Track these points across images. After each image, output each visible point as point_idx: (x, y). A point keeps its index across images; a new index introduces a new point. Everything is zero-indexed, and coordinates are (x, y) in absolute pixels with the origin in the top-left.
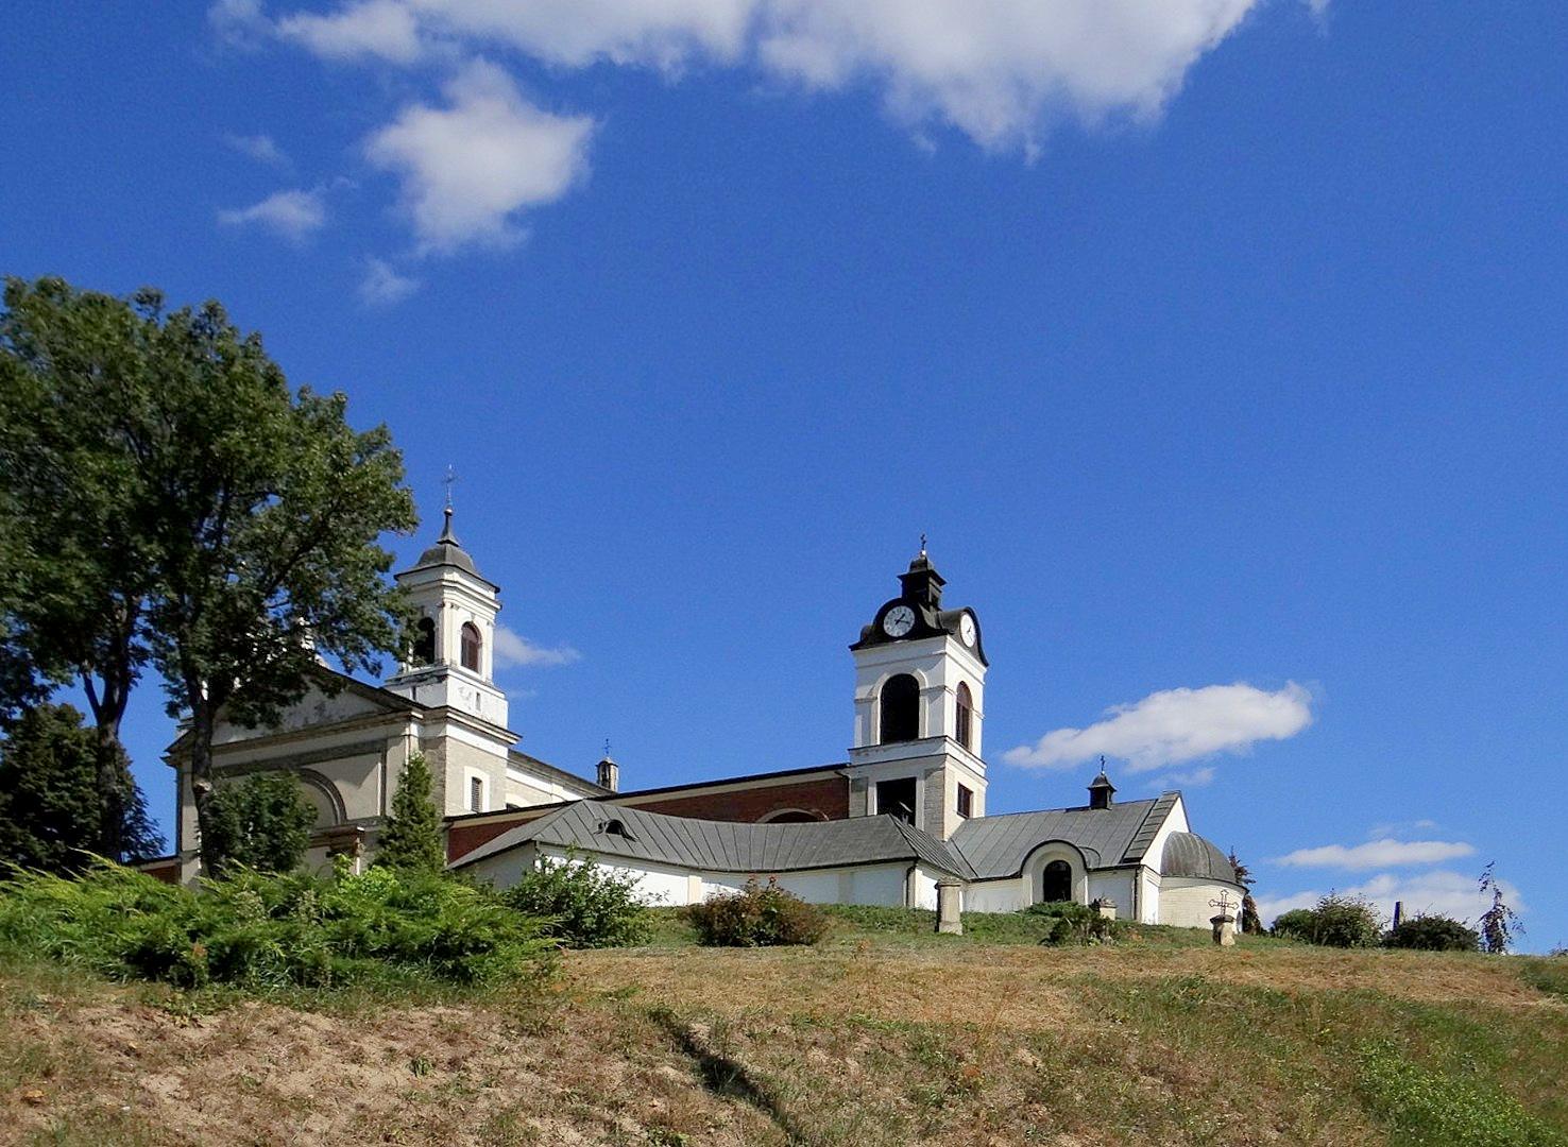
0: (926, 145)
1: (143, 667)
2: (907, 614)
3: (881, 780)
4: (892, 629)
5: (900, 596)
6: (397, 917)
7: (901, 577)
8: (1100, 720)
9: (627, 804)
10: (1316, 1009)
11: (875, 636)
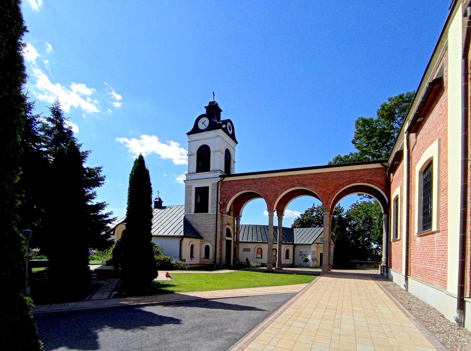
0: (136, 169)
1: (299, 216)
2: (206, 120)
3: (196, 187)
4: (201, 126)
5: (205, 113)
6: (59, 308)
7: (206, 107)
8: (391, 183)
9: (170, 295)
10: (190, 206)
11: (196, 130)
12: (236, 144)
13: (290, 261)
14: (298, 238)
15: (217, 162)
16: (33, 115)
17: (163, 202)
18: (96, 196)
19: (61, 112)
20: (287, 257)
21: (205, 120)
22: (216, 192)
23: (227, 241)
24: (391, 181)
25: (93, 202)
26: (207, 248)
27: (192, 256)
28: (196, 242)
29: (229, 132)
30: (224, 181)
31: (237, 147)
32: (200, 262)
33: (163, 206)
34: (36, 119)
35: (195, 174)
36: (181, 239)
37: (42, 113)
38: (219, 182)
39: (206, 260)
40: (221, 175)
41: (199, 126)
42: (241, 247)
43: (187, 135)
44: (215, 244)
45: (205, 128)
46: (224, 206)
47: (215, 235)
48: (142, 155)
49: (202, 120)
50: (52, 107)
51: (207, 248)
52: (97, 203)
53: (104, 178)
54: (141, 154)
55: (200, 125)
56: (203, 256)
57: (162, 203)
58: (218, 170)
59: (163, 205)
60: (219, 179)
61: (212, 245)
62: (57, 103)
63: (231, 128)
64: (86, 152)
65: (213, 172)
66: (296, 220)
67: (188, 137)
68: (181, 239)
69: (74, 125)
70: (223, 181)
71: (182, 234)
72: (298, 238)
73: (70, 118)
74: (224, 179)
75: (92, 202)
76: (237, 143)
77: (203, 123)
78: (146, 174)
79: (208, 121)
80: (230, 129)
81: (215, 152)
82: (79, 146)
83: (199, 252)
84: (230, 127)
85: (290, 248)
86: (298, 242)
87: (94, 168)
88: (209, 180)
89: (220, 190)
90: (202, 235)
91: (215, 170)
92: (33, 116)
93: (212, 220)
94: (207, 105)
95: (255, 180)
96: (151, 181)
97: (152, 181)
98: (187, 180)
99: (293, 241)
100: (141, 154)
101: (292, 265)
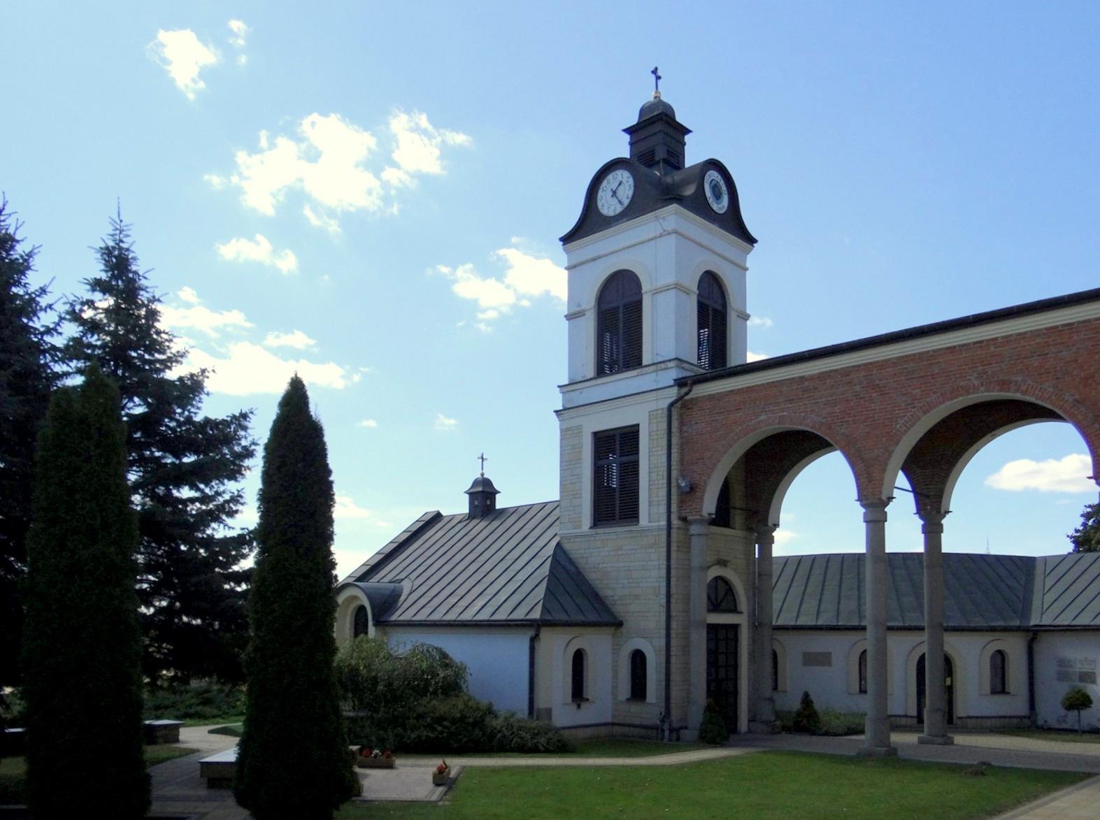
2: (624, 180)
4: (608, 205)
11: (590, 222)
12: (750, 246)
13: (1014, 704)
14: (1049, 598)
15: (668, 330)
16: (29, 292)
17: (499, 492)
18: (242, 504)
19: (130, 257)
20: (1000, 686)
21: (620, 178)
22: (664, 442)
23: (712, 628)
24: (399, 604)
25: (231, 525)
26: (638, 659)
27: (578, 693)
28: (597, 645)
29: (715, 207)
30: (692, 399)
31: (755, 259)
32: (614, 716)
33: (499, 506)
34: (38, 299)
35: (593, 382)
36: (531, 633)
37: (53, 280)
38: (672, 405)
39: (636, 708)
40: (681, 376)
41: (600, 204)
42: (792, 650)
43: (561, 243)
44: (663, 642)
45: (619, 209)
46: (692, 491)
47: (663, 610)
48: (299, 375)
49: (612, 181)
50: (103, 245)
51: (638, 659)
52: (243, 529)
53: (253, 447)
54: (296, 375)
55: (603, 201)
56: (625, 690)
57: (497, 496)
58: (670, 361)
59: (500, 503)
60: (673, 393)
61: (655, 650)
62: (117, 229)
63: (724, 188)
64: (203, 371)
65: (652, 368)
66: (1089, 510)
67: (565, 250)
68: (531, 633)
69: (43, 326)
70: (687, 398)
71: (536, 615)
72: (1049, 598)
73: (153, 269)
74: (690, 391)
75: (230, 528)
76: (751, 241)
77: (614, 193)
78: (313, 433)
79: (631, 181)
80: (718, 196)
81: (657, 292)
82: (182, 356)
83: (609, 675)
84: (715, 188)
85: (1015, 647)
86: (1046, 620)
87: (229, 419)
88: (640, 401)
89: (677, 434)
90: (619, 609)
91: (660, 359)
92: (30, 295)
93: (653, 550)
94: (633, 120)
95: (807, 384)
96: (260, 486)
97: (332, 461)
98: (568, 406)
99: (1025, 611)
100: (296, 375)
101: (1026, 721)
